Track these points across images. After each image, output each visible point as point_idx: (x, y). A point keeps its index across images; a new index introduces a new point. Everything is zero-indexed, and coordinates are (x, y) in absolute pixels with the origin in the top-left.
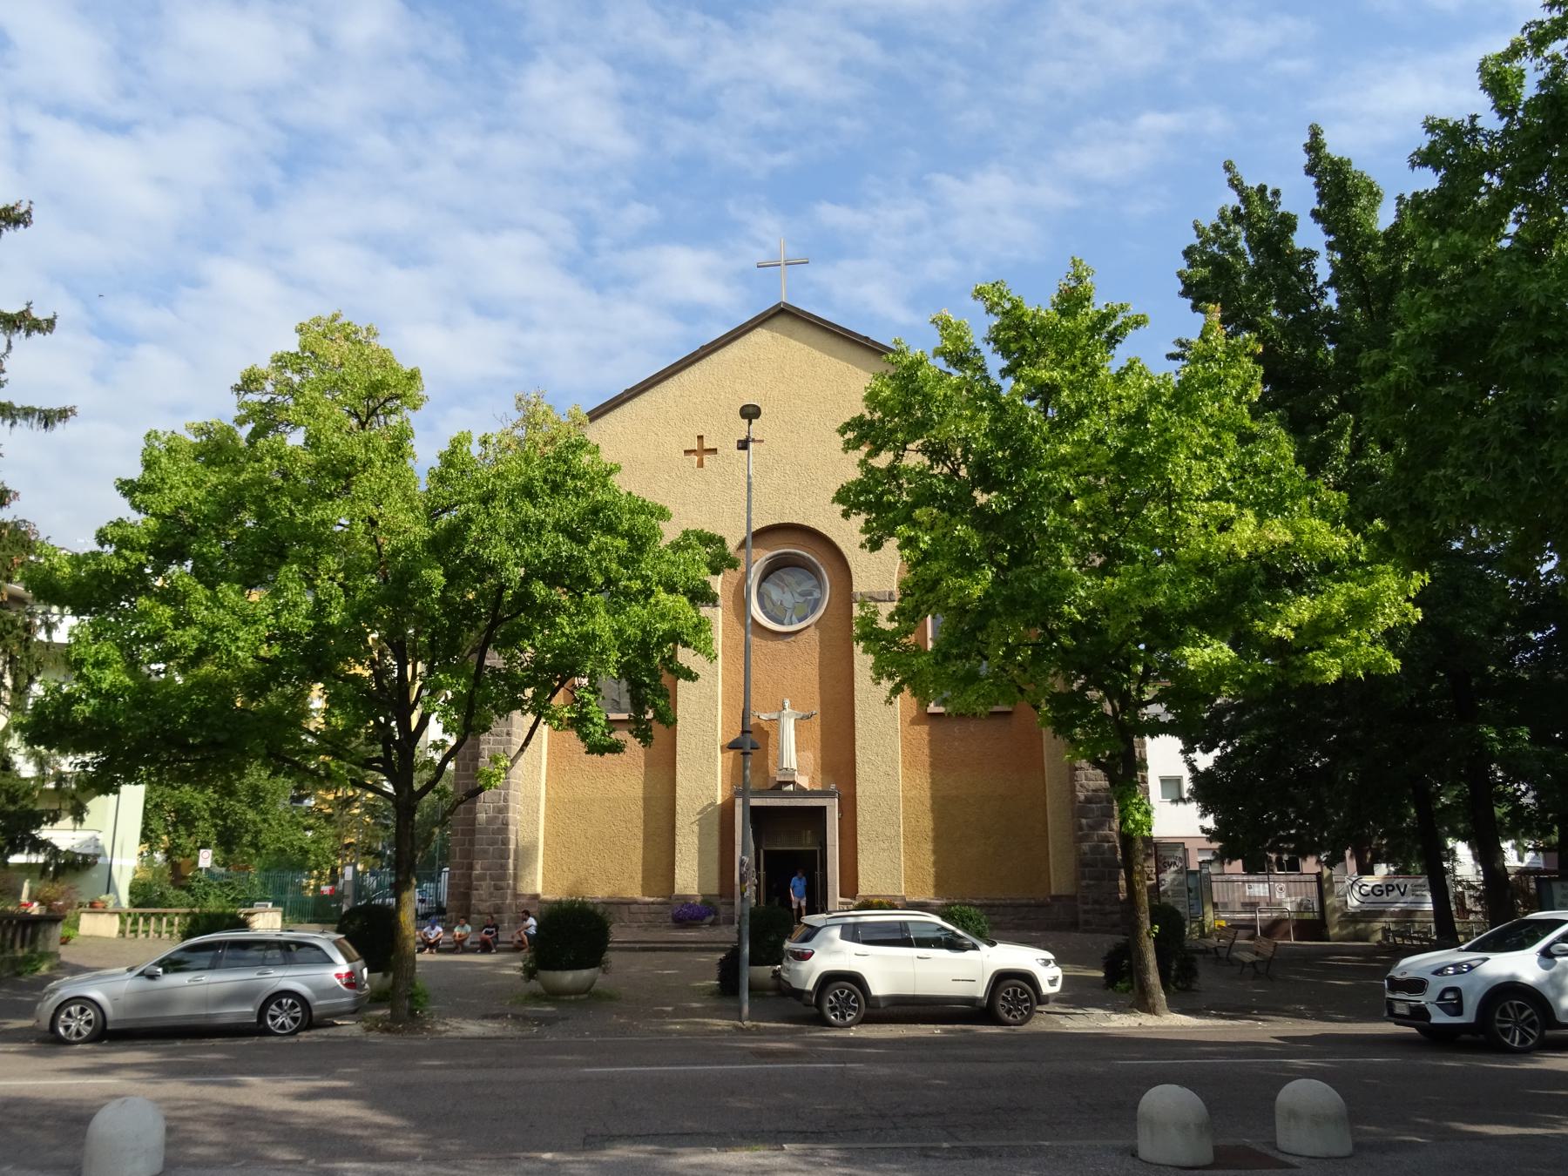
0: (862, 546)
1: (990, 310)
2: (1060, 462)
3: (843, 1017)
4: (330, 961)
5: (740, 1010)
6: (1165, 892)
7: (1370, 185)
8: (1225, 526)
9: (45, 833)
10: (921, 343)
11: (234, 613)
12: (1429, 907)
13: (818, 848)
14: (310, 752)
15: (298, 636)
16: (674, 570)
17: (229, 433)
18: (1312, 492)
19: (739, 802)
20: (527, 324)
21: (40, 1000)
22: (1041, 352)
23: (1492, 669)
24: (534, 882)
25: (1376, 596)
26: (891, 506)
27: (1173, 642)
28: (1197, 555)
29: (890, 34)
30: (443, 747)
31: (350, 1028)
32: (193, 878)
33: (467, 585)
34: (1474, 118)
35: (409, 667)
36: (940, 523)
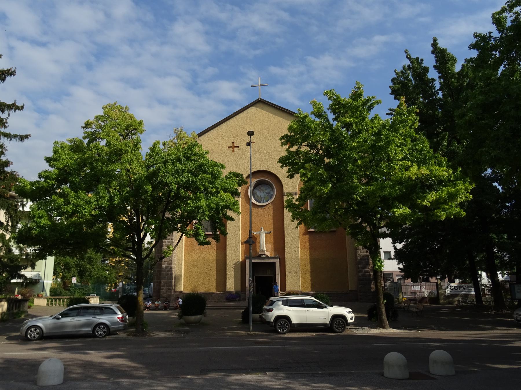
0: (287, 177)
1: (329, 99)
2: (353, 149)
3: (283, 330)
4: (116, 313)
5: (249, 328)
6: (387, 289)
7: (453, 57)
8: (407, 169)
9: (23, 272)
10: (306, 110)
11: (84, 200)
12: (473, 293)
13: (273, 276)
14: (109, 245)
15: (104, 208)
16: (226, 185)
17: (81, 142)
18: (436, 158)
19: (248, 261)
20: (176, 106)
21: (22, 326)
22: (346, 113)
23: (494, 215)
24: (181, 287)
25: (457, 191)
26: (297, 164)
27: (390, 207)
28: (398, 178)
29: (293, 11)
30: (152, 243)
31: (122, 335)
32: (70, 287)
33: (159, 191)
34: (490, 33)
35: (140, 218)
36: (314, 169)
